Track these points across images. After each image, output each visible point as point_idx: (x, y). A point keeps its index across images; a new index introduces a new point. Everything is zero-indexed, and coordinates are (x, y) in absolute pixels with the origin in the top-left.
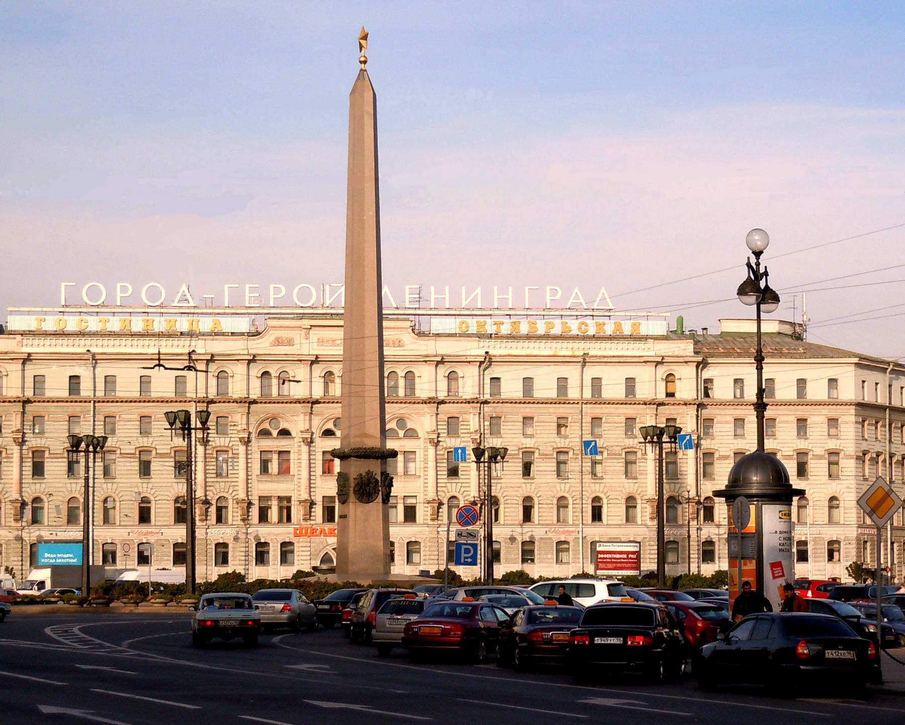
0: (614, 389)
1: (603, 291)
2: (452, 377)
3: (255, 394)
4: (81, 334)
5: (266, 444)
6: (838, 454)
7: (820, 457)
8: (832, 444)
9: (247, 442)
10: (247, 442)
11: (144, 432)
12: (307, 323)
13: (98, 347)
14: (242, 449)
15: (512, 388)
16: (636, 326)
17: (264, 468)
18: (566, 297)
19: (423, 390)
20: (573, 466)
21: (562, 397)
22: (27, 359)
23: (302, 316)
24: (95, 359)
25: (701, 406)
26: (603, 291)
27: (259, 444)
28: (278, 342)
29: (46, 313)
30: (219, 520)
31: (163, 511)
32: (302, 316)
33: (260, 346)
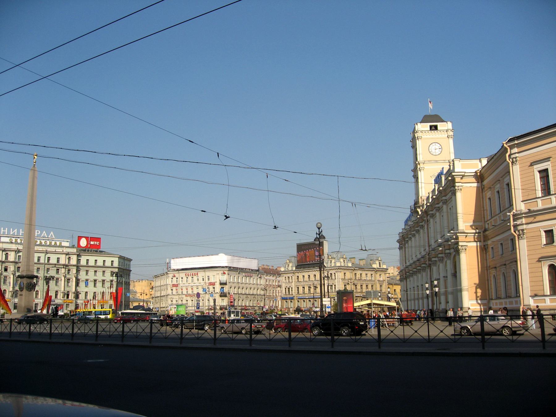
1: (52, 233)
13: (49, 249)
16: (61, 243)
18: (41, 233)
24: (47, 253)
26: (52, 233)
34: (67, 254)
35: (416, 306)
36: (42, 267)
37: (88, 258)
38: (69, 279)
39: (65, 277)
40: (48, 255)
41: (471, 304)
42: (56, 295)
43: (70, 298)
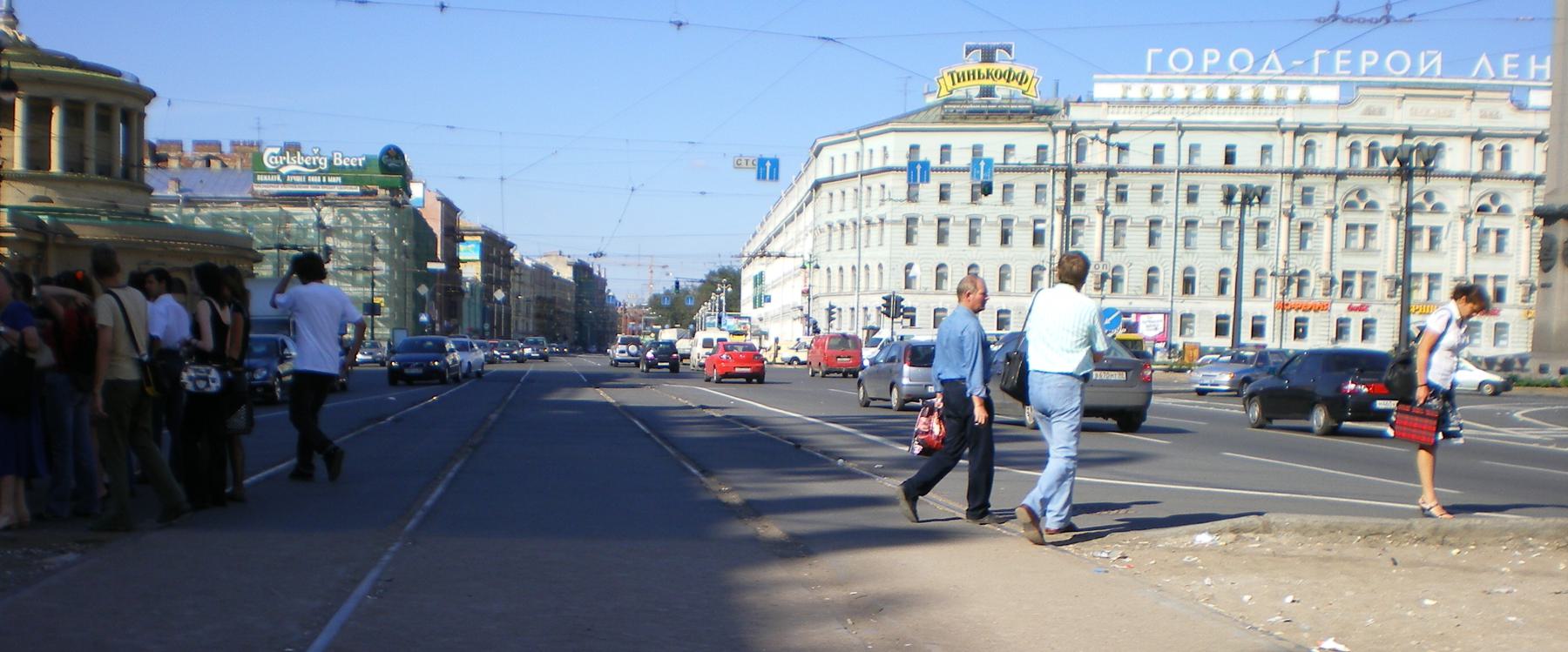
0: (1212, 155)
1: (1484, 59)
2: (1309, 146)
3: (1343, 165)
4: (1167, 103)
5: (1352, 217)
6: (947, 220)
7: (930, 223)
8: (1155, 211)
9: (1334, 217)
10: (1334, 217)
11: (1192, 198)
12: (1400, 92)
13: (1182, 116)
14: (1327, 221)
15: (1140, 156)
17: (1479, 246)
19: (1519, 165)
20: (1166, 235)
21: (1040, 165)
22: (1113, 129)
23: (1394, 86)
24: (1182, 129)
25: (1070, 173)
26: (1484, 59)
27: (1344, 218)
28: (1369, 112)
29: (1218, 81)
30: (1114, 289)
31: (1206, 281)
32: (1394, 86)
33: (1352, 117)
34: (1299, 132)
35: (1169, 401)
36: (1169, 183)
37: (1009, 138)
38: (1305, 226)
39: (1105, 213)
40: (1189, 138)
41: (247, 482)
42: (1003, 278)
43: (1308, 292)
